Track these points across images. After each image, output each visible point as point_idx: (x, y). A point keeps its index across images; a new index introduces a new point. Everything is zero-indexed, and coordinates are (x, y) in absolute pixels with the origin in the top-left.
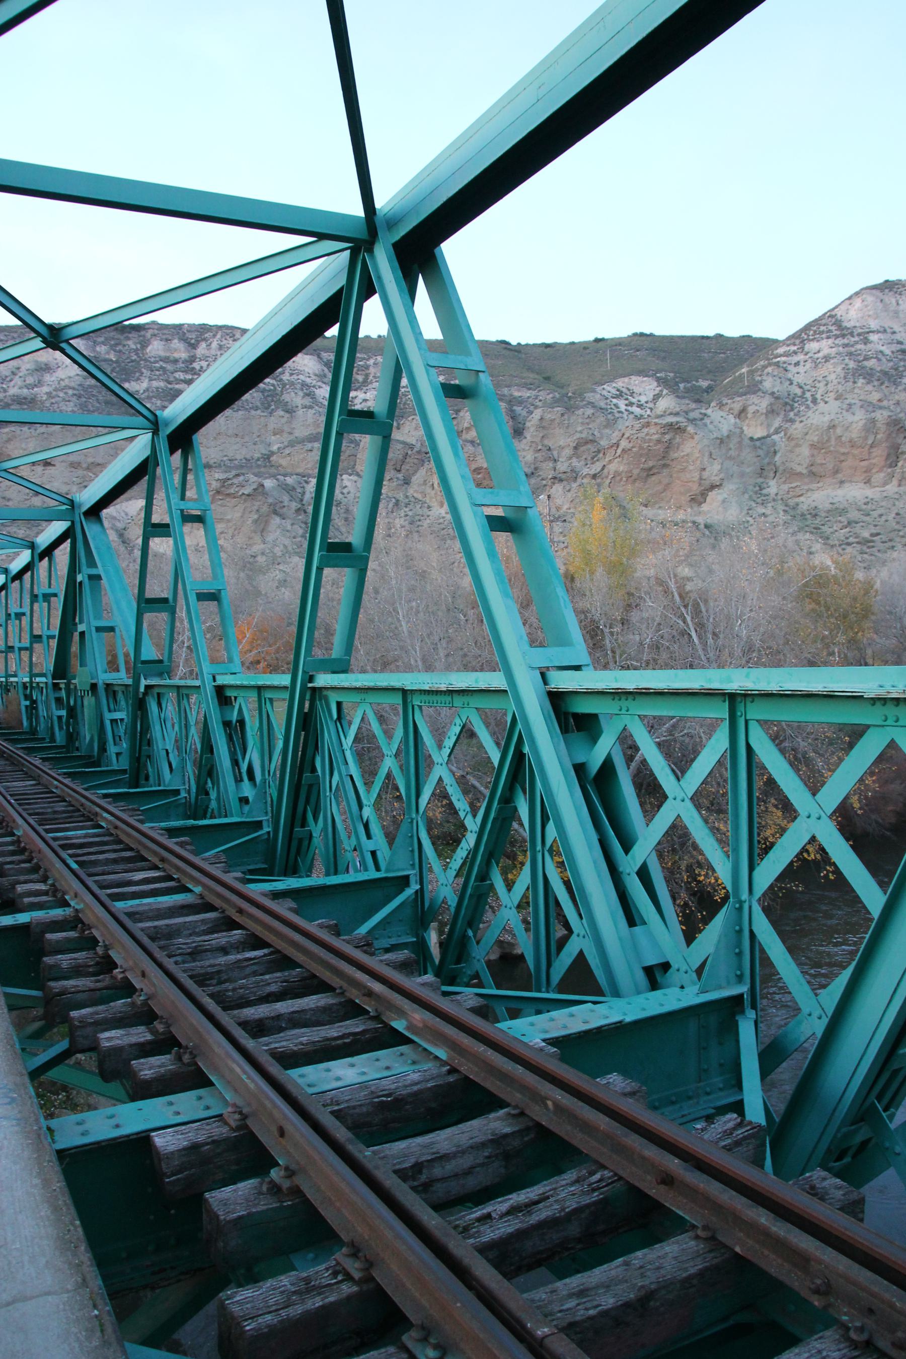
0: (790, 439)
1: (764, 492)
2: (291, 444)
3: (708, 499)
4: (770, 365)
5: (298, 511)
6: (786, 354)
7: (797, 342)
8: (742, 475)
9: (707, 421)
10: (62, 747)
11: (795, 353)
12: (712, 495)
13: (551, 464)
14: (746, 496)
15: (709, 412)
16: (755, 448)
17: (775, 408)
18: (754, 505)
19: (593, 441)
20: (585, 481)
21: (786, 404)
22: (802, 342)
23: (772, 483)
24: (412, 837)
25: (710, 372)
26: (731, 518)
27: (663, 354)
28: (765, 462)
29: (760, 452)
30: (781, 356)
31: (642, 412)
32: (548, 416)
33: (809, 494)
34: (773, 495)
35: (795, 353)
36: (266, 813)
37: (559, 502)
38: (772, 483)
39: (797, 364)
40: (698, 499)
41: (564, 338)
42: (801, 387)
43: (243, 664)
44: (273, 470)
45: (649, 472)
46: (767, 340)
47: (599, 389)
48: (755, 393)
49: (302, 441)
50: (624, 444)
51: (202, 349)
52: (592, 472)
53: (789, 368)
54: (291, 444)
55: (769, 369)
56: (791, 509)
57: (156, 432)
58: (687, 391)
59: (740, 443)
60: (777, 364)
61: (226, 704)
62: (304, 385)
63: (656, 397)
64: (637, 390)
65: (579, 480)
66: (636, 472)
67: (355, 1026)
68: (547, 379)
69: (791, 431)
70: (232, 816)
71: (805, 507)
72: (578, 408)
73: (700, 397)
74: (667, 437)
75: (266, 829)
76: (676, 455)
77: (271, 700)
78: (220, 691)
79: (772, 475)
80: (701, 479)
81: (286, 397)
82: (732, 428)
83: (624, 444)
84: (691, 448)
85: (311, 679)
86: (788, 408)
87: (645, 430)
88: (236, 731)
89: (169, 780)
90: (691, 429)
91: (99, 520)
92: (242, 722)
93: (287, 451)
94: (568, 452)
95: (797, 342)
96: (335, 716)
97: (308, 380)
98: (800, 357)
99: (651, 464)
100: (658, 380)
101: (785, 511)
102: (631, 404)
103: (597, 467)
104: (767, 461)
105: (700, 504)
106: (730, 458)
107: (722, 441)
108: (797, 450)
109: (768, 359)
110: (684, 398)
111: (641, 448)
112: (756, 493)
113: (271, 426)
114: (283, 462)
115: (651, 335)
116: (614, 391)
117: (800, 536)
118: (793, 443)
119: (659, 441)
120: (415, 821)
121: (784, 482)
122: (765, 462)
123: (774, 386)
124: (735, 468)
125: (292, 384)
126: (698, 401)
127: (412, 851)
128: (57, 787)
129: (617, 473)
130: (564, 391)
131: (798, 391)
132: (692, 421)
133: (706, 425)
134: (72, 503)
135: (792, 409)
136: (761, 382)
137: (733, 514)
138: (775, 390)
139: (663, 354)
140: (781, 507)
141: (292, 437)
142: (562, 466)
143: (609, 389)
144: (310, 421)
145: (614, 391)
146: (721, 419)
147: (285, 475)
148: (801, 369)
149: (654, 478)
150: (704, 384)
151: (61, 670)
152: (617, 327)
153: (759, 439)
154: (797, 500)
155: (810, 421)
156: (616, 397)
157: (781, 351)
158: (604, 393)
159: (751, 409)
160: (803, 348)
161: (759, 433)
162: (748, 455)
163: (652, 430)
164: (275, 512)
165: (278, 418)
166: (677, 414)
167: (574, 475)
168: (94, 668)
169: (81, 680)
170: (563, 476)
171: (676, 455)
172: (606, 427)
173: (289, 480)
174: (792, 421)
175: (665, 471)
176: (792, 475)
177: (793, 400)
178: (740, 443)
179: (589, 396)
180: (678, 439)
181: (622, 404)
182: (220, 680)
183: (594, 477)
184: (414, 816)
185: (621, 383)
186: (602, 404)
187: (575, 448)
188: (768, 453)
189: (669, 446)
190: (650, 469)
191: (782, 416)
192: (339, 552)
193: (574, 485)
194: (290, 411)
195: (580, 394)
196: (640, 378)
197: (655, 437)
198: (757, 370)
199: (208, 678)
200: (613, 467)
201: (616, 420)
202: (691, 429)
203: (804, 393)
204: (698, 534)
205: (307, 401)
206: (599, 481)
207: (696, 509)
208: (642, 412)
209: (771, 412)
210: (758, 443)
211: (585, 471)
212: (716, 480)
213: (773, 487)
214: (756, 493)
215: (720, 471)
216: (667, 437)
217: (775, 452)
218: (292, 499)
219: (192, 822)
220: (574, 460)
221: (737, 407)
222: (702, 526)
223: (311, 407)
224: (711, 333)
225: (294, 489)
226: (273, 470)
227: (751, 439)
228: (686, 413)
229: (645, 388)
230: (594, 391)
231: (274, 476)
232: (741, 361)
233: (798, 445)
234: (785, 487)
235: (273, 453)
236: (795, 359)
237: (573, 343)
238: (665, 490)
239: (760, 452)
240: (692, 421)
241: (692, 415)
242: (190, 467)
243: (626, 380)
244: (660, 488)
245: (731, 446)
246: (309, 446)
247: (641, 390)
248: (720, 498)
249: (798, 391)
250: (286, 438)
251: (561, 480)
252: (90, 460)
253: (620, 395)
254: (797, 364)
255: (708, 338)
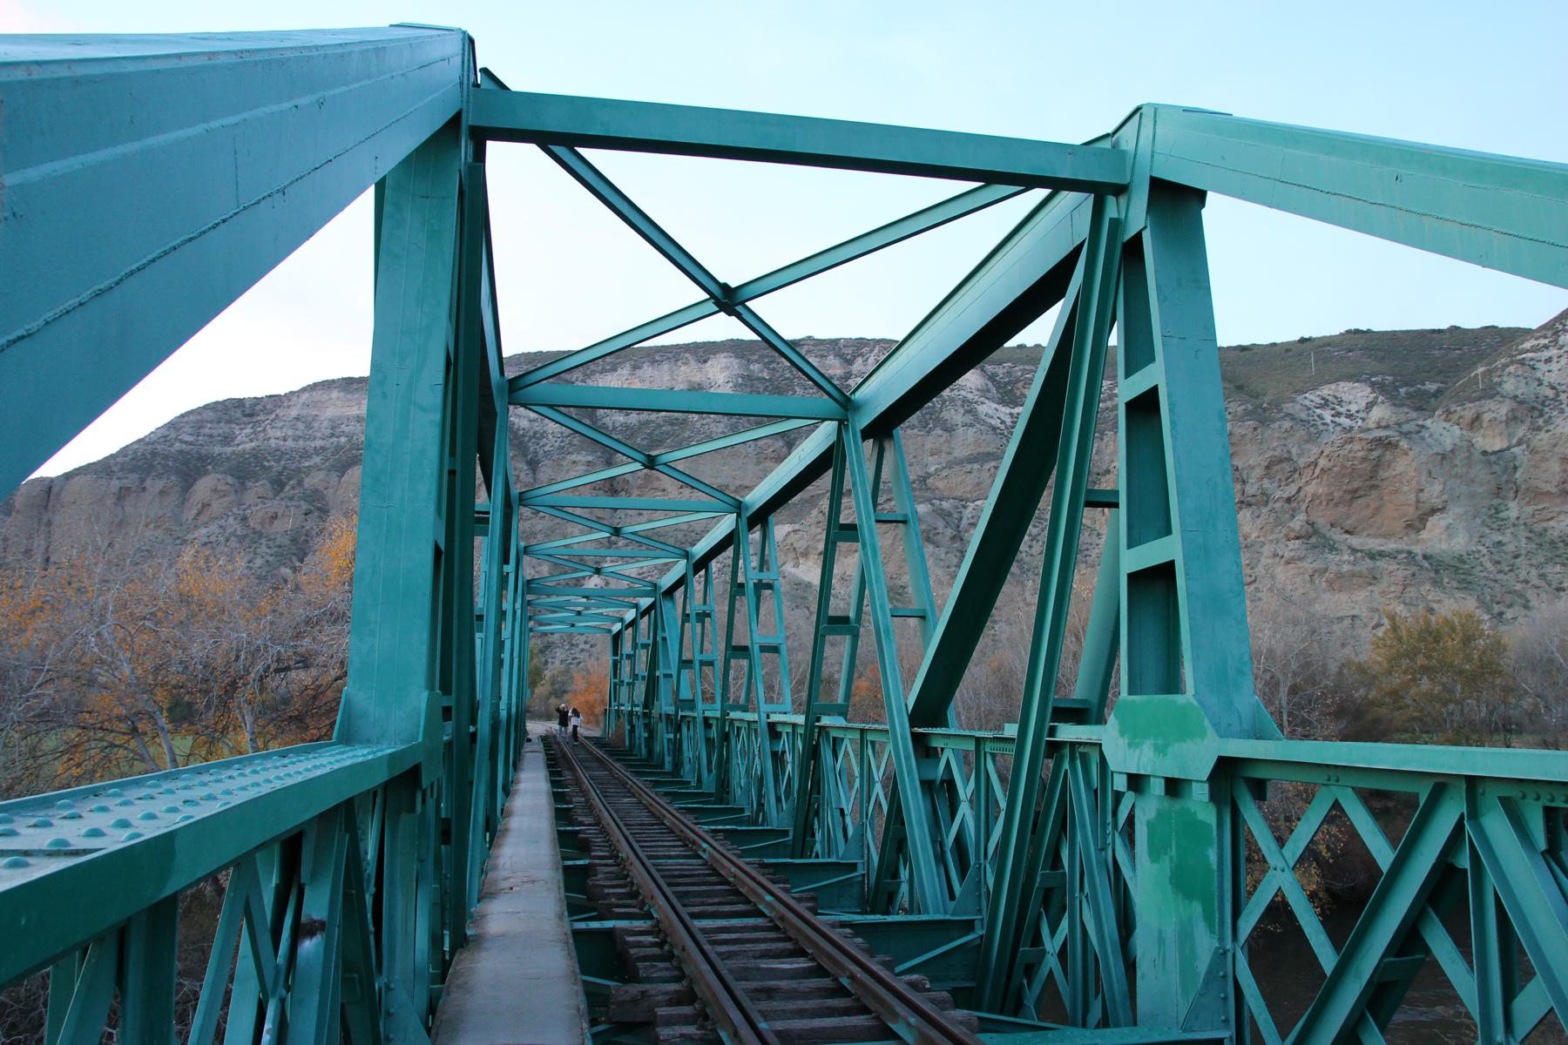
0: (1533, 451)
1: (1502, 515)
2: (949, 465)
3: (1428, 525)
4: (1512, 363)
5: (953, 538)
6: (1533, 350)
7: (1549, 333)
8: (1472, 495)
9: (1425, 434)
10: (710, 795)
11: (1546, 347)
12: (1433, 520)
13: (1239, 486)
14: (1478, 521)
15: (1428, 423)
16: (1489, 463)
17: (1518, 414)
18: (1487, 531)
19: (1289, 459)
20: (1278, 505)
21: (1533, 408)
22: (1556, 333)
23: (1513, 505)
24: (1225, 977)
25: (1440, 372)
26: (1458, 547)
27: (1381, 354)
28: (1503, 478)
29: (1496, 468)
30: (1527, 351)
31: (1353, 423)
32: (1238, 431)
33: (1562, 517)
34: (1512, 520)
35: (1546, 347)
36: (980, 911)
37: (1246, 529)
38: (1513, 505)
39: (1548, 360)
40: (1417, 524)
41: (1263, 338)
42: (1553, 388)
43: (793, 702)
44: (928, 494)
45: (1354, 495)
46: (1518, 330)
47: (1299, 398)
48: (1492, 397)
49: (960, 462)
50: (1322, 462)
51: (858, 366)
52: (1286, 495)
53: (1538, 365)
54: (949, 465)
55: (1512, 369)
56: (1538, 537)
57: (739, 515)
58: (1409, 396)
59: (1469, 458)
60: (1522, 362)
61: (927, 756)
62: (965, 401)
63: (1370, 406)
64: (1345, 397)
65: (1271, 504)
66: (1337, 495)
67: (788, 945)
68: (1240, 388)
69: (1535, 442)
70: (927, 912)
71: (1556, 534)
72: (1273, 421)
73: (1423, 403)
74: (1375, 454)
75: (860, 871)
76: (1387, 474)
77: (873, 743)
78: (772, 727)
79: (1512, 495)
80: (1418, 501)
81: (945, 415)
82: (1457, 441)
83: (1322, 462)
84: (1404, 465)
85: (818, 720)
86: (1536, 413)
87: (1348, 447)
88: (941, 792)
89: (841, 853)
90: (1404, 444)
91: (672, 598)
92: (950, 784)
93: (944, 473)
94: (1259, 472)
95: (1549, 333)
96: (1542, 845)
97: (970, 396)
98: (1553, 352)
99: (1355, 485)
100: (1373, 385)
101: (1528, 538)
102: (1339, 414)
103: (1291, 490)
104: (1505, 478)
105: (1419, 531)
106: (1456, 476)
107: (1444, 457)
108: (1544, 465)
109: (1511, 356)
110: (1402, 405)
111: (1343, 467)
112: (1491, 517)
113: (928, 446)
114: (940, 485)
115: (1369, 331)
116: (1318, 400)
117: (1549, 569)
118: (1538, 457)
119: (1364, 459)
120: (1229, 955)
121: (1528, 503)
122: (1503, 478)
123: (1517, 388)
124: (1463, 487)
125: (952, 400)
126: (1419, 409)
127: (1225, 999)
128: (768, 904)
129: (1315, 497)
130: (1258, 402)
131: (1550, 393)
132: (1406, 435)
133: (1423, 439)
134: (655, 586)
135: (1541, 415)
136: (1500, 384)
137: (1459, 543)
138: (1519, 393)
139: (1381, 354)
140: (1522, 533)
141: (951, 458)
142: (1251, 489)
143: (1313, 397)
144: (971, 440)
145: (1318, 400)
146: (1443, 431)
147: (941, 500)
148: (1554, 366)
149: (1359, 501)
150: (1432, 387)
151: (649, 702)
152: (1327, 324)
153: (1494, 453)
154: (1545, 525)
155: (1559, 430)
156: (1321, 407)
157: (1527, 345)
158: (1307, 402)
159: (1487, 417)
160: (1556, 341)
161: (1498, 444)
162: (1480, 471)
163: (1356, 446)
164: (928, 540)
165: (937, 437)
166: (1387, 427)
167: (1265, 498)
168: (665, 705)
169: (655, 712)
170: (1252, 500)
171: (1387, 474)
172: (1307, 441)
173: (945, 505)
174: (1539, 429)
175: (1374, 493)
176: (1538, 494)
177: (1543, 404)
178: (1469, 458)
179: (1288, 407)
180: (1388, 456)
181: (1327, 415)
182: (774, 718)
183: (1289, 500)
184: (1229, 946)
185: (1326, 391)
186: (1303, 416)
187: (1267, 467)
188: (1505, 471)
189: (1378, 464)
190: (1356, 491)
191: (1527, 424)
192: (840, 623)
193: (1264, 510)
194: (949, 429)
195: (1277, 404)
196: (1350, 384)
197: (1360, 454)
198: (1496, 369)
199: (764, 716)
200: (1310, 489)
201: (1319, 433)
202: (1404, 444)
203: (1557, 395)
204: (1414, 569)
205: (969, 419)
206: (1294, 505)
207: (1413, 536)
208: (1353, 423)
209: (1513, 419)
210: (1493, 458)
211: (1278, 494)
212: (1438, 502)
213: (1513, 510)
214: (1491, 517)
215: (1443, 492)
216: (1375, 454)
217: (1515, 468)
218: (947, 525)
219: (878, 918)
220: (1266, 481)
221: (1469, 412)
222: (1419, 558)
223: (972, 425)
224: (1444, 326)
225: (950, 514)
226: (928, 494)
227: (1485, 453)
228: (1399, 425)
229: (1356, 395)
230: (1293, 401)
231: (929, 500)
232: (1481, 357)
233: (1544, 459)
234: (1530, 509)
235: (929, 475)
236: (1546, 354)
237: (1274, 344)
238: (1374, 515)
239: (1496, 468)
240: (1406, 435)
241: (1406, 428)
242: (847, 484)
243: (1333, 386)
244: (1368, 512)
245: (1457, 462)
246: (969, 467)
247: (1351, 398)
248: (1443, 523)
249: (1550, 393)
250: (944, 459)
251: (1250, 505)
252: (738, 483)
253: (1325, 403)
254: (1548, 360)
255: (1440, 331)
